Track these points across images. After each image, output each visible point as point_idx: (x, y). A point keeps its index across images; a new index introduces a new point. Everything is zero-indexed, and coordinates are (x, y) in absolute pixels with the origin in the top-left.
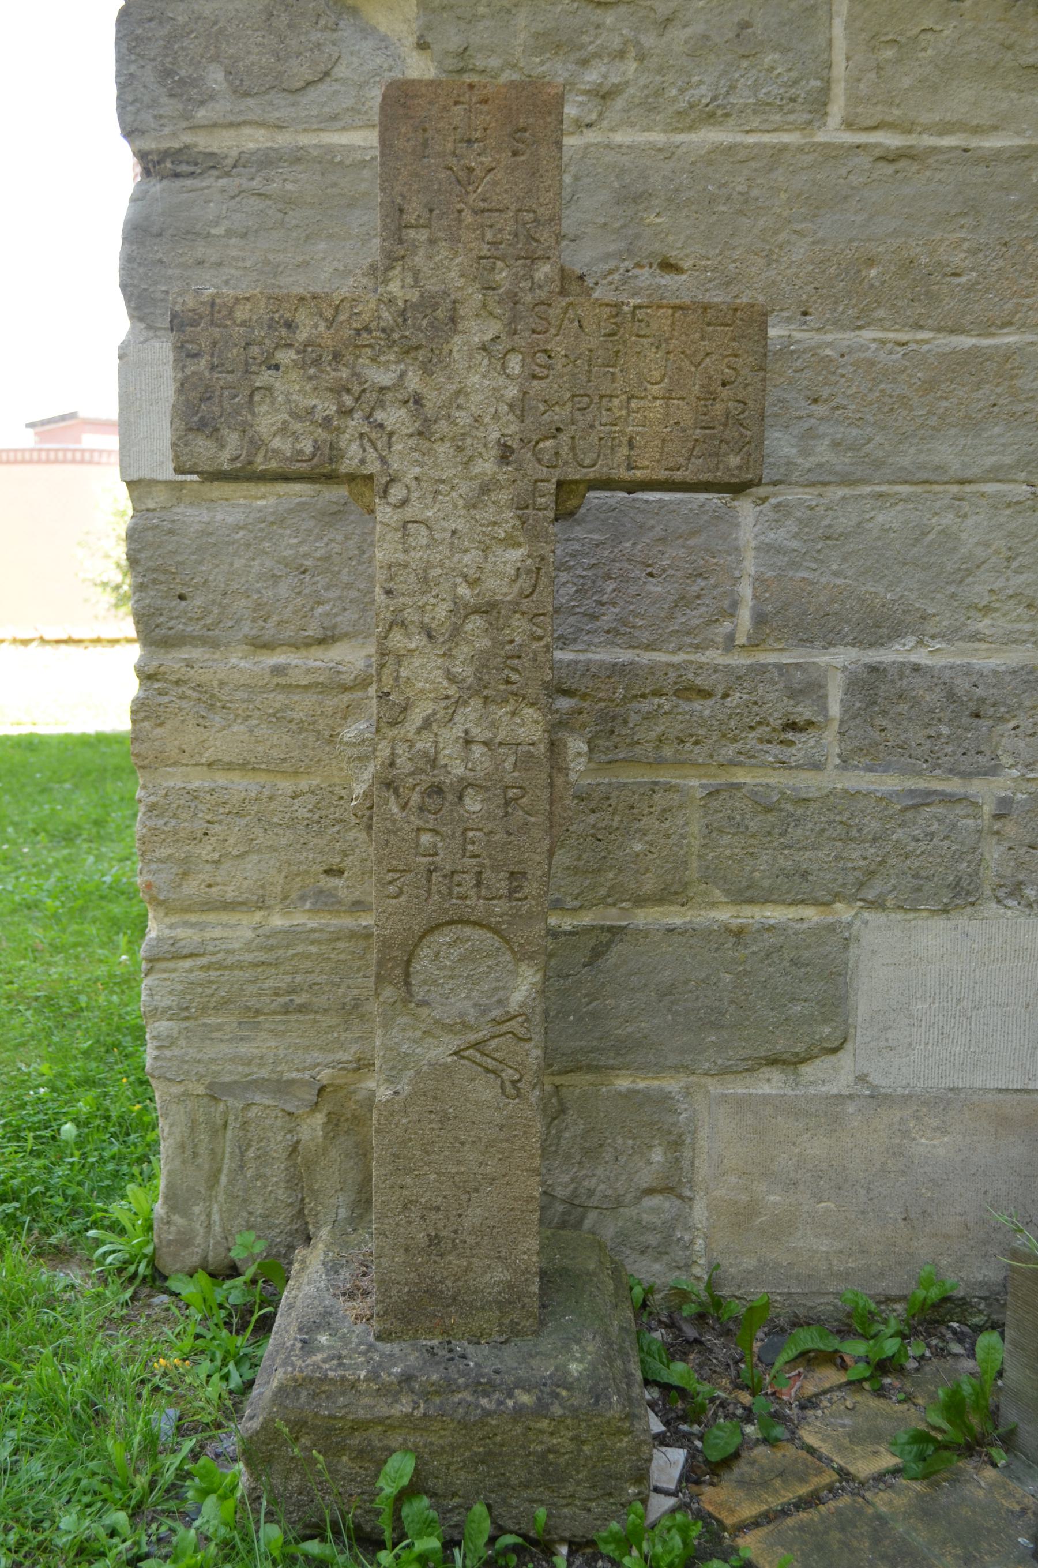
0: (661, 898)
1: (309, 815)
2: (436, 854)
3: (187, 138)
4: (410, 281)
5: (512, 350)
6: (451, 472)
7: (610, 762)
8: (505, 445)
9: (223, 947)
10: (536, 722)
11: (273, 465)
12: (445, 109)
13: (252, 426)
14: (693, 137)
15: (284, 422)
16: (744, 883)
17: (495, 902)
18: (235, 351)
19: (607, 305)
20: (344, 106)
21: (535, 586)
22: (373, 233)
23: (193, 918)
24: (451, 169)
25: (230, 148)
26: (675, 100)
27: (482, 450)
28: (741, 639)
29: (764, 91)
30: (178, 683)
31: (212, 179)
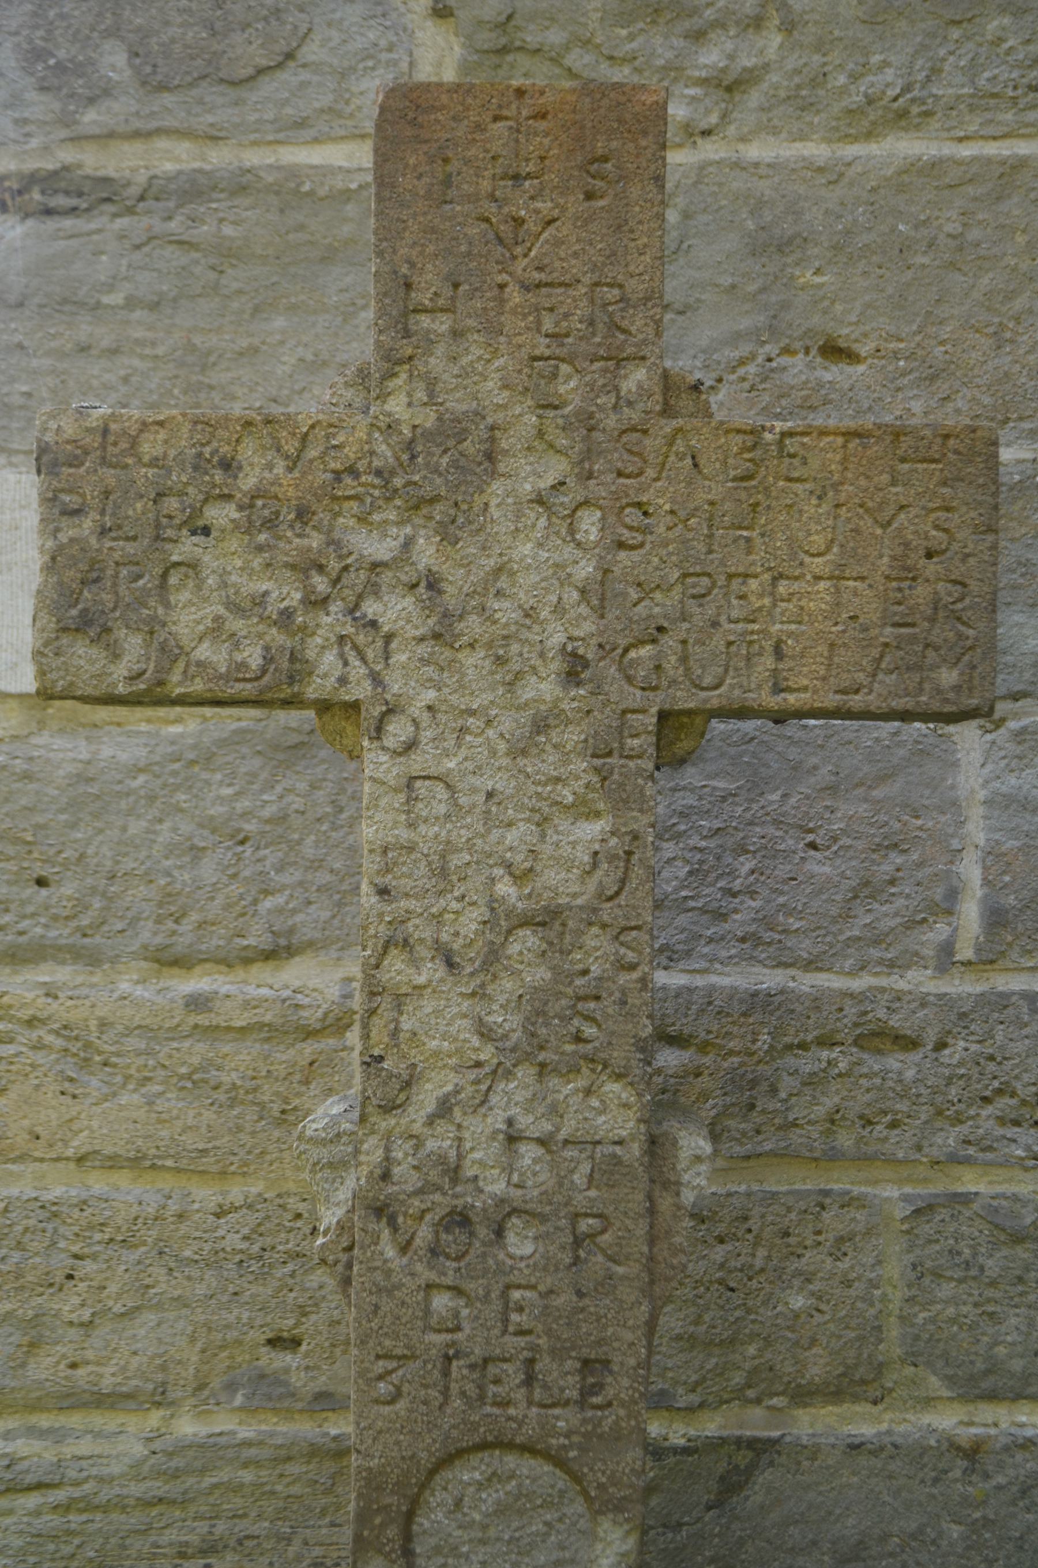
0: (839, 1390)
1: (244, 1246)
2: (458, 1328)
3: (67, 155)
4: (421, 395)
5: (586, 503)
6: (487, 697)
7: (748, 1158)
8: (574, 654)
9: (94, 1471)
10: (626, 1106)
11: (198, 686)
12: (479, 127)
13: (164, 625)
14: (874, 148)
15: (217, 619)
16: (980, 1366)
17: (557, 1411)
18: (139, 506)
19: (739, 431)
20: (317, 105)
21: (623, 882)
22: (360, 302)
23: (44, 1420)
24: (487, 220)
25: (134, 170)
26: (843, 91)
27: (536, 662)
28: (965, 952)
29: (986, 75)
30: (31, 1023)
31: (105, 219)
